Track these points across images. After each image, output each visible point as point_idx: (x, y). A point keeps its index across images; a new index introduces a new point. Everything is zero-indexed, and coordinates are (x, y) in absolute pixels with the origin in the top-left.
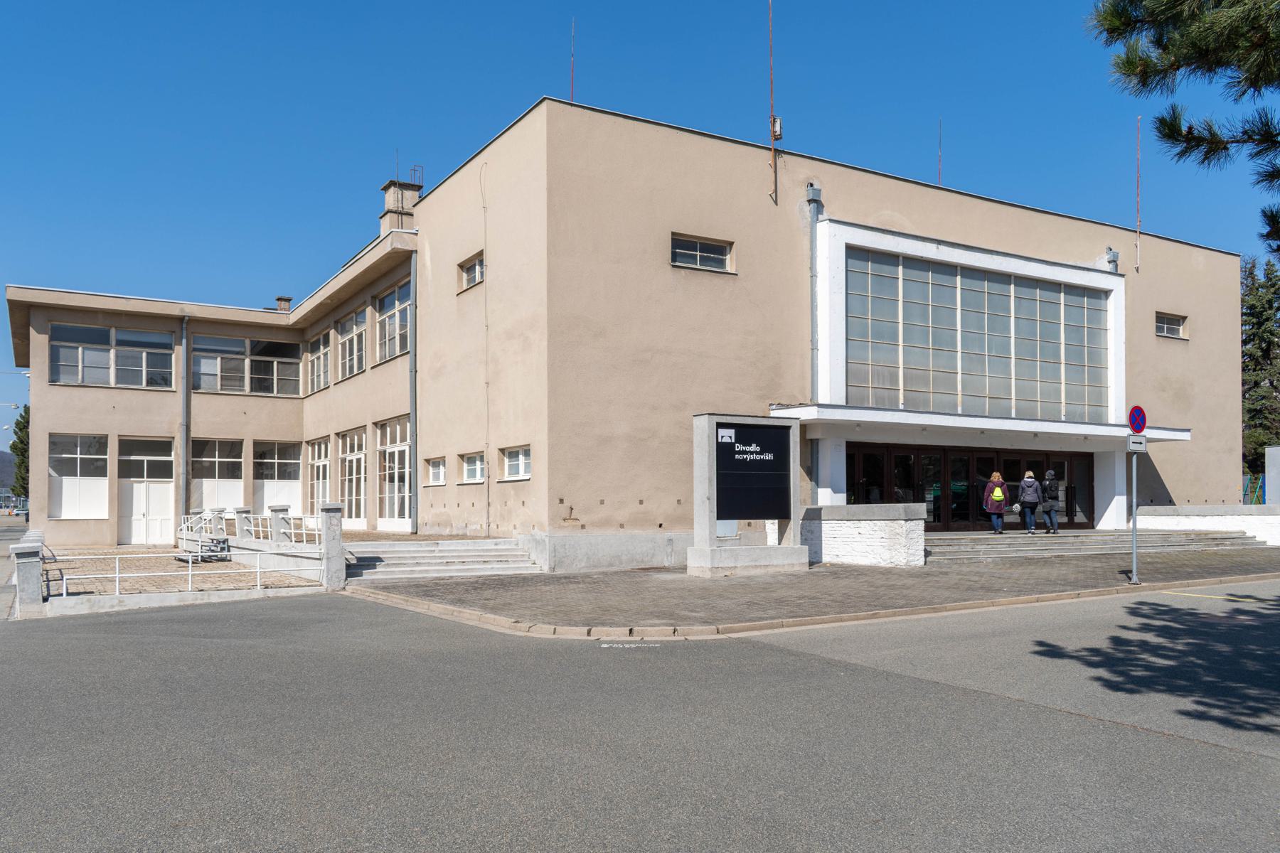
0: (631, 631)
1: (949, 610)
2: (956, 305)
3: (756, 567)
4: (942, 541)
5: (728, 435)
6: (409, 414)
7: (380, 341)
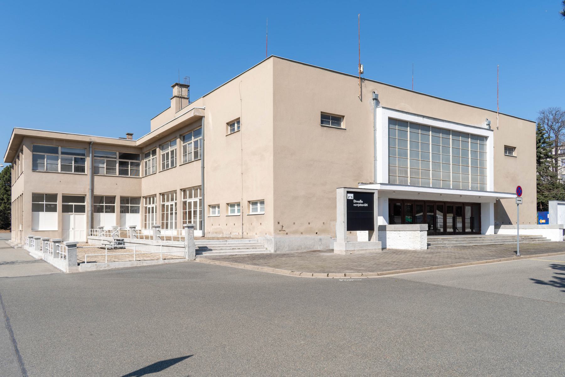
0: (328, 275)
1: (456, 266)
2: (407, 139)
3: (362, 250)
4: (431, 239)
5: (351, 196)
6: (201, 185)
7: (183, 154)
